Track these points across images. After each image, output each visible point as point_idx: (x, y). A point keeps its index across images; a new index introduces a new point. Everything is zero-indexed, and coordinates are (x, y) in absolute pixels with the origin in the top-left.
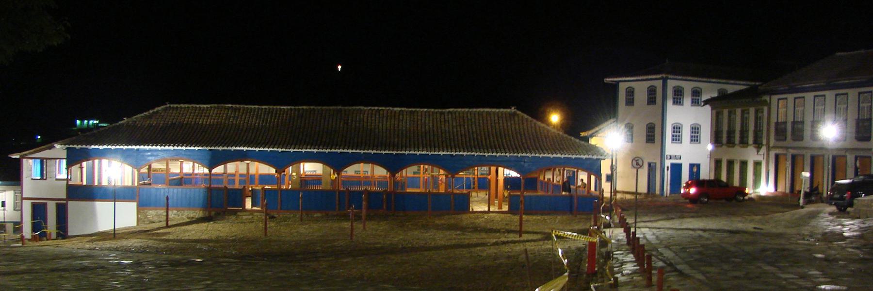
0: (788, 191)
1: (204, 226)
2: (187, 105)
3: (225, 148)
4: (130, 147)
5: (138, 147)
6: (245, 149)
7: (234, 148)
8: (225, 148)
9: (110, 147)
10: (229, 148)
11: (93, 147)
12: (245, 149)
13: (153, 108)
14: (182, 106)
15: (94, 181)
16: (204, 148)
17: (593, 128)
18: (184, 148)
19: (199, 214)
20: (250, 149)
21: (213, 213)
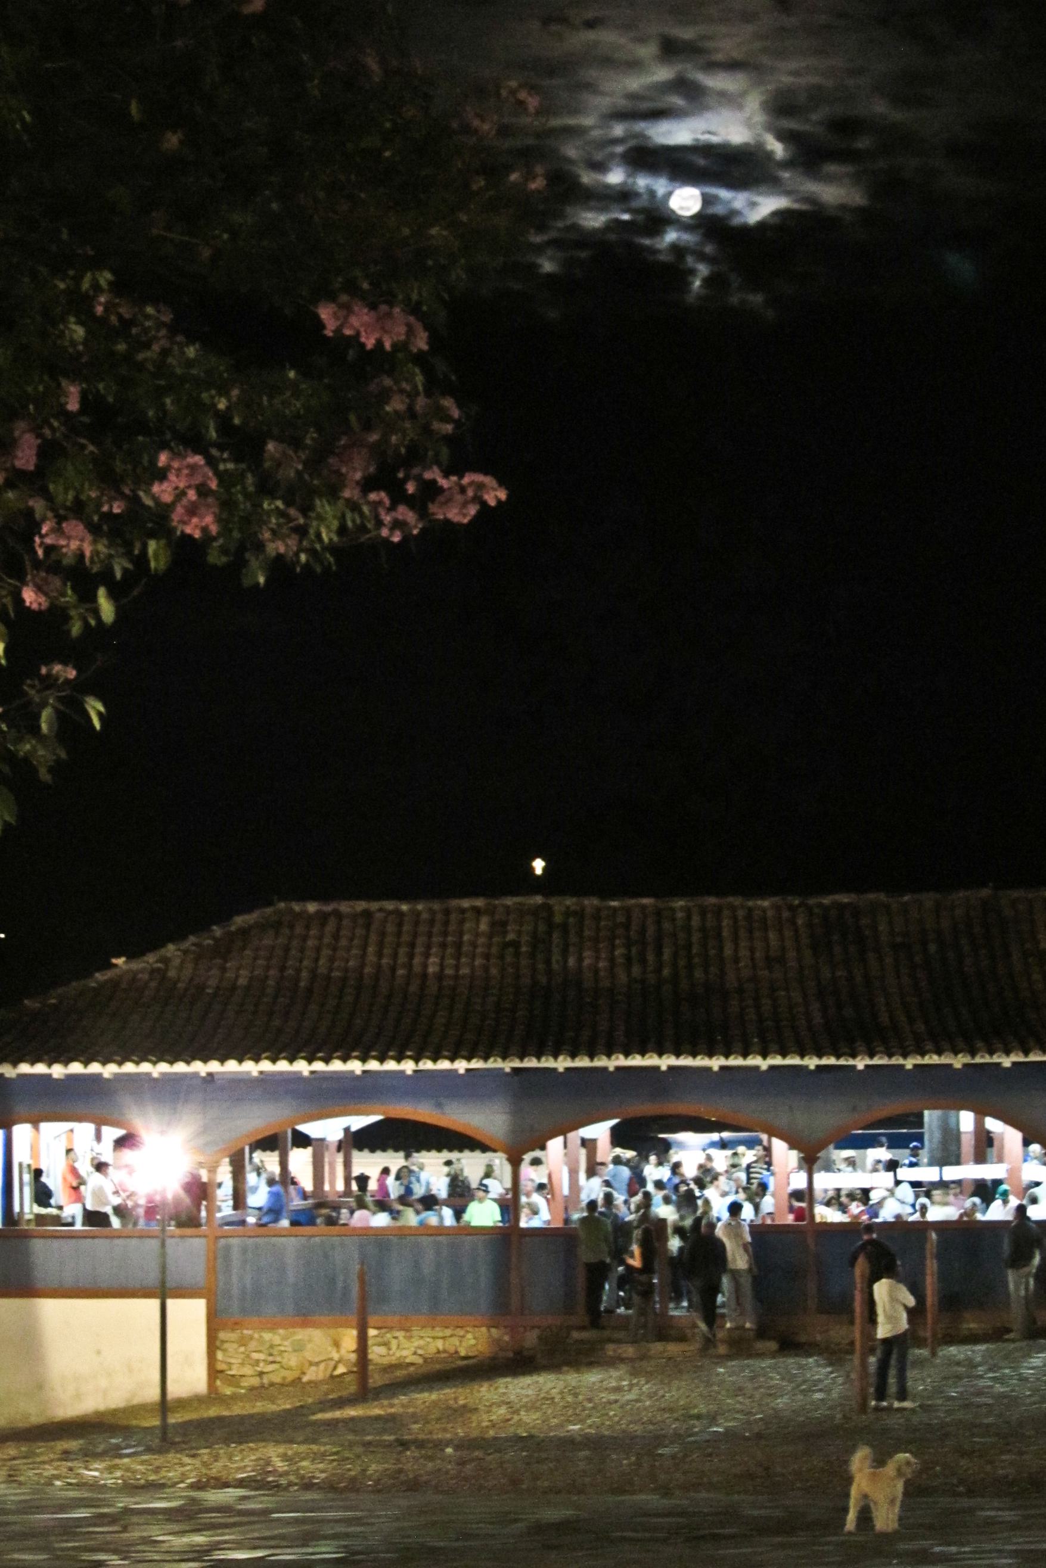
0: (848, 169)
1: (546, 1383)
2: (361, 905)
3: (583, 1062)
4: (180, 1067)
5: (214, 1066)
6: (666, 1062)
7: (620, 1061)
8: (583, 1062)
9: (145, 1067)
10: (601, 1062)
11: (25, 1068)
12: (666, 1062)
13: (224, 918)
14: (345, 907)
15: (1041, 1062)
16: (495, 1063)
17: (925, 1295)
18: (408, 1066)
19: (471, 1341)
20: (686, 1061)
21: (531, 1339)
